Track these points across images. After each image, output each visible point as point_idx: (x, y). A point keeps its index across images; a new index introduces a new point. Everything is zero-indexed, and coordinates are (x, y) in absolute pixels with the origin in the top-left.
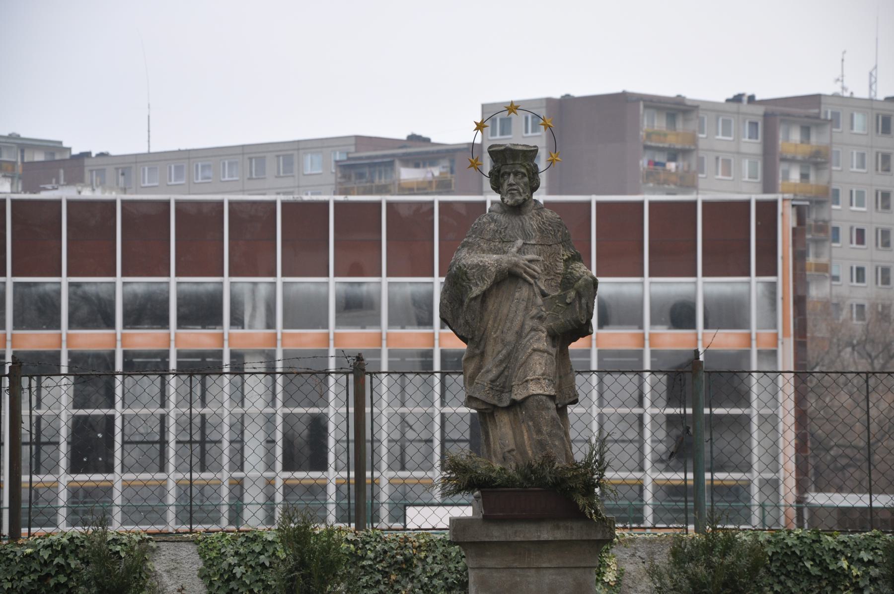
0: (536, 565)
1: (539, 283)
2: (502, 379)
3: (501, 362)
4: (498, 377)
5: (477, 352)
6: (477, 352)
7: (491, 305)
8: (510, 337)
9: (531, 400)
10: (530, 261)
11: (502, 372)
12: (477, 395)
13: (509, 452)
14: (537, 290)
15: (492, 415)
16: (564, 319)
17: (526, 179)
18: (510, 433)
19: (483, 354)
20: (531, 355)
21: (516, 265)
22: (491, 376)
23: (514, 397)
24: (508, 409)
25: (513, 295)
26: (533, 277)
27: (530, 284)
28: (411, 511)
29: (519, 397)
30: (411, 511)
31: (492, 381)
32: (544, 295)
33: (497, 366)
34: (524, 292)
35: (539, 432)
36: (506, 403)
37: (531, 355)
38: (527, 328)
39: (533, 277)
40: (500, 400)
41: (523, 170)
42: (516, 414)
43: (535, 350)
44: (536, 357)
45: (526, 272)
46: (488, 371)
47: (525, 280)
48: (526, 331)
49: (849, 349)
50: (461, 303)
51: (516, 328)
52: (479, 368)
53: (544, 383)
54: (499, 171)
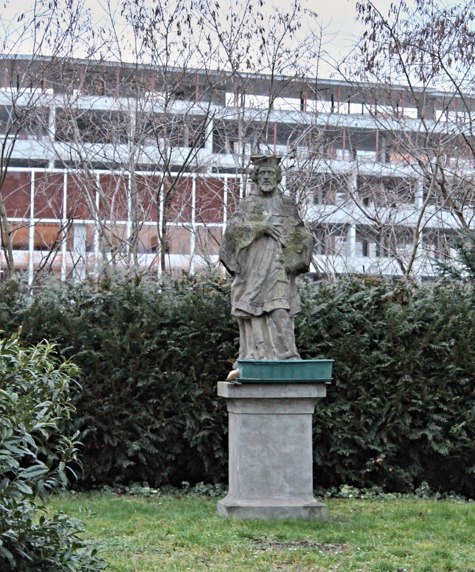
0: (277, 412)
1: (281, 240)
2: (258, 299)
3: (258, 288)
4: (255, 297)
5: (242, 281)
6: (242, 281)
7: (252, 253)
8: (263, 272)
9: (276, 312)
10: (276, 226)
11: (257, 295)
12: (241, 308)
13: (260, 343)
14: (279, 244)
15: (249, 321)
16: (295, 262)
17: (275, 176)
18: (261, 332)
19: (245, 283)
20: (276, 284)
21: (268, 228)
22: (251, 296)
23: (265, 309)
24: (259, 317)
25: (265, 247)
26: (277, 235)
27: (276, 240)
28: (325, 395)
29: (268, 310)
30: (325, 395)
31: (252, 300)
32: (283, 247)
33: (255, 290)
34: (271, 244)
35: (280, 331)
36: (259, 313)
37: (276, 284)
38: (273, 268)
39: (277, 235)
40: (256, 311)
41: (274, 170)
42: (265, 321)
43: (279, 281)
44: (280, 285)
45: (274, 233)
46: (249, 293)
47: (273, 238)
48: (273, 269)
49: (319, 262)
50: (234, 251)
51: (266, 267)
52: (242, 292)
53: (284, 301)
54: (258, 170)
